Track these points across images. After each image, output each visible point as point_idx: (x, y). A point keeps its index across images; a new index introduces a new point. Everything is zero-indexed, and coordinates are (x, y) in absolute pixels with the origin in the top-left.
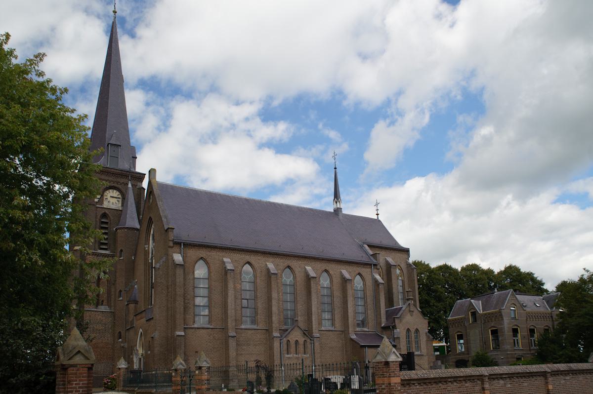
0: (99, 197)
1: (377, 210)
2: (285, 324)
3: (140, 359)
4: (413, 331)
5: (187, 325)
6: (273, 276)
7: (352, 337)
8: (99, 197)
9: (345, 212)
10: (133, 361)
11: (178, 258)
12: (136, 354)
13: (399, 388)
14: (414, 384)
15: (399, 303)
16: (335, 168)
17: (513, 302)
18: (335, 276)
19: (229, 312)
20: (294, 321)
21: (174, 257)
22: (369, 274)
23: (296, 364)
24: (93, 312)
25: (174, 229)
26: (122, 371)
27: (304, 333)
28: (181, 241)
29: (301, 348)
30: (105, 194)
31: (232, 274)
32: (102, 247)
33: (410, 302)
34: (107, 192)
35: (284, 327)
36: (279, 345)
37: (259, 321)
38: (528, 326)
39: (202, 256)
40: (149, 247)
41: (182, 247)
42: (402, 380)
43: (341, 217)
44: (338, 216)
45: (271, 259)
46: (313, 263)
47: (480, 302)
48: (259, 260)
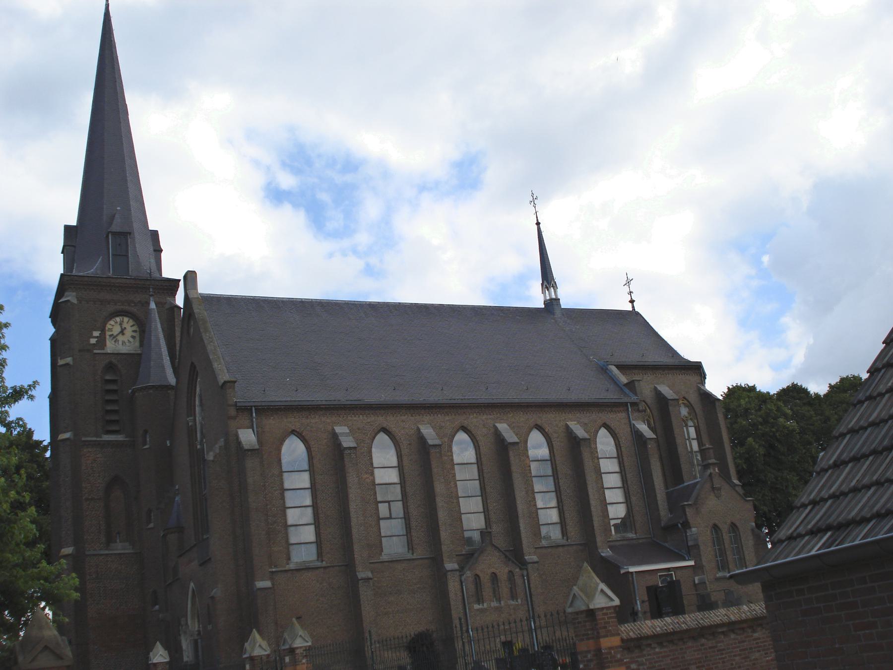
0: (96, 334)
1: (631, 293)
3: (196, 642)
5: (276, 566)
7: (602, 554)
8: (96, 334)
9: (565, 304)
10: (181, 647)
13: (619, 656)
14: (650, 645)
15: (693, 474)
16: (538, 224)
18: (555, 435)
19: (354, 531)
21: (241, 436)
22: (625, 424)
25: (235, 382)
29: (505, 590)
30: (108, 326)
33: (712, 471)
34: (112, 322)
36: (459, 587)
39: (293, 428)
40: (195, 420)
41: (254, 414)
42: (622, 640)
43: (558, 314)
44: (554, 314)
45: (427, 418)
48: (403, 421)
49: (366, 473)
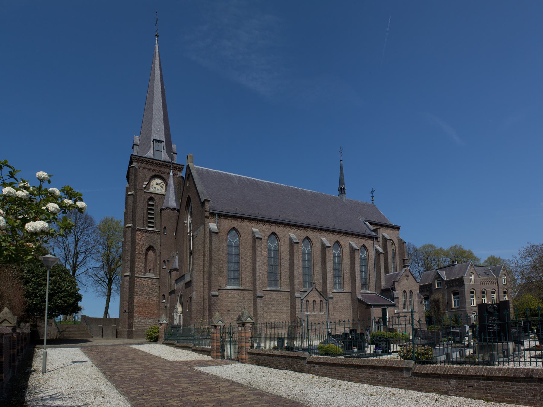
0: (146, 183)
2: (304, 286)
3: (180, 316)
4: (408, 292)
6: (295, 245)
7: (358, 298)
11: (213, 226)
12: (176, 312)
17: (472, 271)
20: (312, 284)
21: (210, 226)
23: (283, 322)
24: (142, 279)
26: (163, 325)
27: (321, 294)
28: (216, 212)
31: (260, 242)
32: (149, 225)
35: (303, 289)
37: (283, 283)
38: (481, 289)
41: (217, 217)
45: (293, 230)
46: (327, 235)
47: (444, 272)
49: (264, 251)
